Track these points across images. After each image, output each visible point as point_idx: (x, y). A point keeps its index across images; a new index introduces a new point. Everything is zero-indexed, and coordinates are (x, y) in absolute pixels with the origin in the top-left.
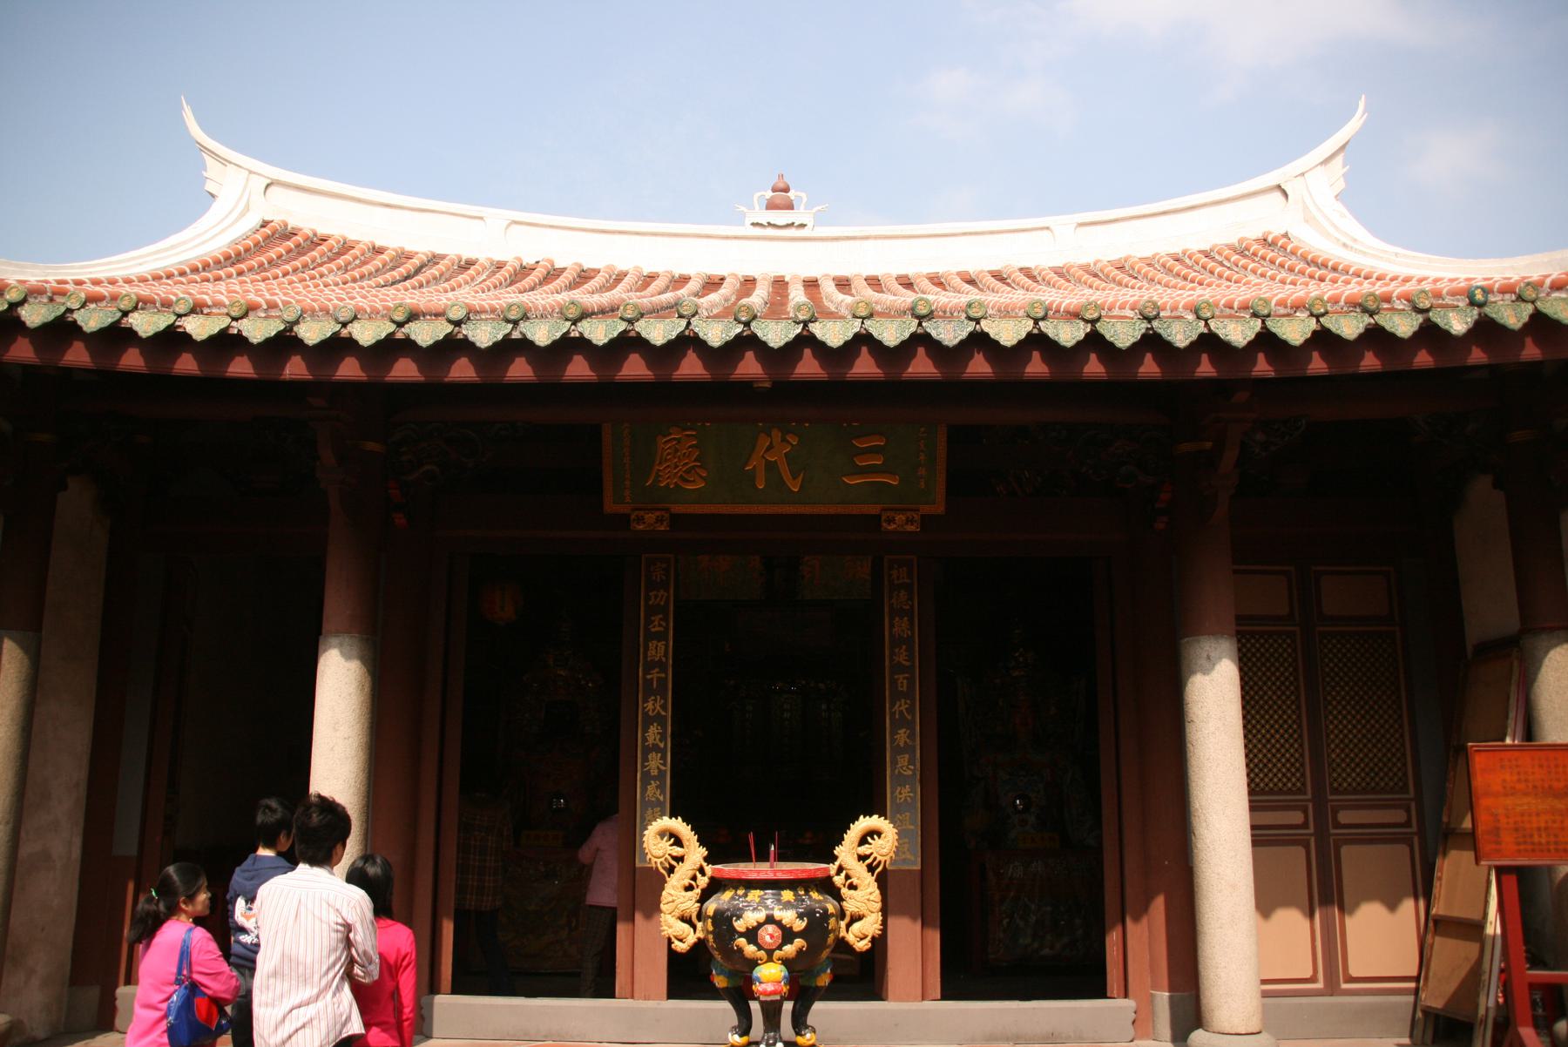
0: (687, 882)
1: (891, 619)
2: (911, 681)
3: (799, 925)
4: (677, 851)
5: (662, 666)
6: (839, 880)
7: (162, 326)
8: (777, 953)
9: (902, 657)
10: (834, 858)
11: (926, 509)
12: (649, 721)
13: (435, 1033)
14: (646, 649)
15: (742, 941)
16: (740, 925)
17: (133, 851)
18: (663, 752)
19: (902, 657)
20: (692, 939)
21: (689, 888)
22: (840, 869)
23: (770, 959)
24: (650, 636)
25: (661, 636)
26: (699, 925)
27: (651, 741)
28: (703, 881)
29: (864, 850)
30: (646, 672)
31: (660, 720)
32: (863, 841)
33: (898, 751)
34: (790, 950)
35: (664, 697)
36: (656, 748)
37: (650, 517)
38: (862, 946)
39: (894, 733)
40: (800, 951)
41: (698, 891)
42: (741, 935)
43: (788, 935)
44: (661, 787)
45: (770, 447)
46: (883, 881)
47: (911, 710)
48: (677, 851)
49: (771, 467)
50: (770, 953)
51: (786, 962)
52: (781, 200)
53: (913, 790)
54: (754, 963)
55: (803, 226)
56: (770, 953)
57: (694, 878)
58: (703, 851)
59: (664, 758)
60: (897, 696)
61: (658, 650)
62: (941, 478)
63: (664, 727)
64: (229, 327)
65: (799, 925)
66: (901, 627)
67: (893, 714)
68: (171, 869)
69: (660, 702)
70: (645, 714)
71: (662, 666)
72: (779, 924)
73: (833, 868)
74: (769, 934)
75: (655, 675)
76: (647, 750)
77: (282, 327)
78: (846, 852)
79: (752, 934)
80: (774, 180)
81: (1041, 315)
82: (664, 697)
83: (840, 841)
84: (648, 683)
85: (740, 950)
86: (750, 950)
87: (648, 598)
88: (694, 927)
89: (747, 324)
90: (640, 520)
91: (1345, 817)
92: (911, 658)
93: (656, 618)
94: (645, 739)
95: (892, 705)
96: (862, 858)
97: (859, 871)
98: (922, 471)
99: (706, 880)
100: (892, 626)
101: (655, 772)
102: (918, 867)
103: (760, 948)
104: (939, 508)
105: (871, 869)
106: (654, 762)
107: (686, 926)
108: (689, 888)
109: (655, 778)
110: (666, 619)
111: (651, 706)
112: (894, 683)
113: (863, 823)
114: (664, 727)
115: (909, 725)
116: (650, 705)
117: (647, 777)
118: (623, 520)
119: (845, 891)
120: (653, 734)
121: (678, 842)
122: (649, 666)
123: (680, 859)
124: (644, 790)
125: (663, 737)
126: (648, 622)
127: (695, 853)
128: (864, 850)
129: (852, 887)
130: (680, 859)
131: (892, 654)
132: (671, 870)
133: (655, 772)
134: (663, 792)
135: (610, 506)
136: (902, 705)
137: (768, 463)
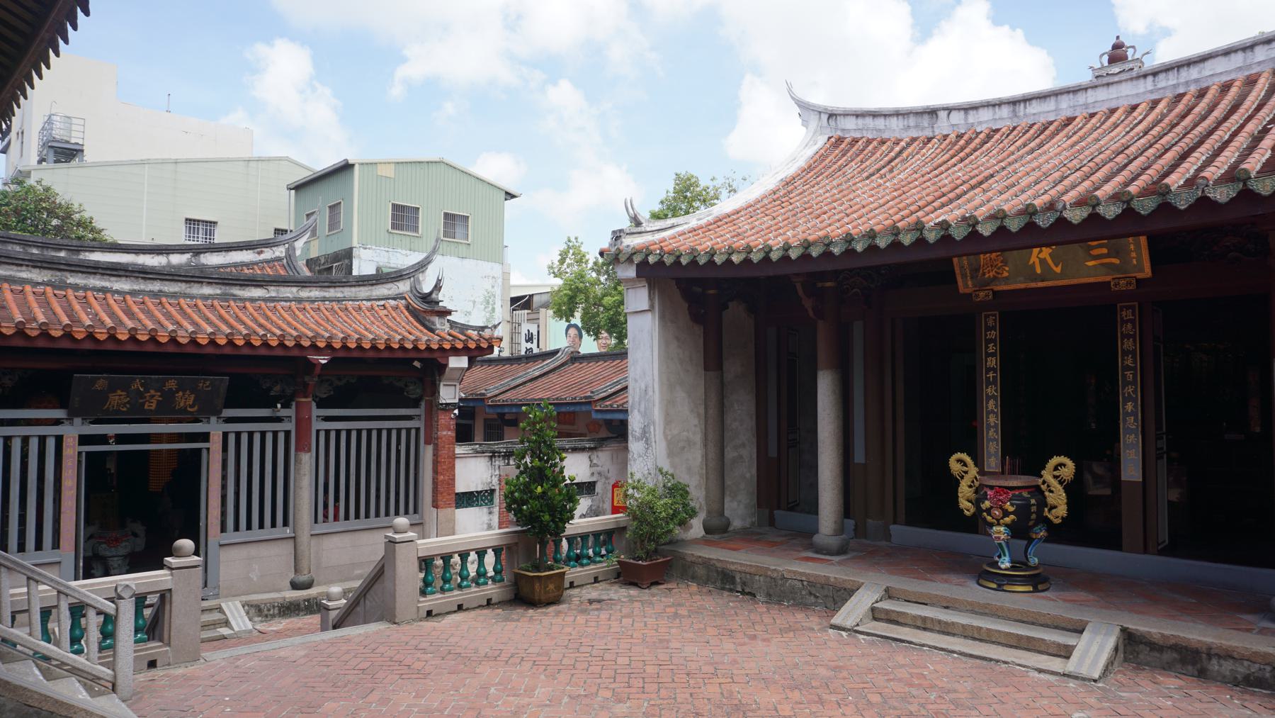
2: (1135, 376)
4: (965, 469)
5: (994, 370)
6: (1044, 487)
9: (1129, 362)
11: (1140, 276)
12: (989, 398)
13: (346, 246)
17: (775, 455)
19: (1129, 362)
22: (1044, 482)
23: (999, 524)
24: (988, 355)
25: (993, 355)
28: (977, 484)
29: (1056, 473)
32: (1056, 469)
33: (1127, 414)
36: (992, 412)
37: (982, 294)
38: (1058, 521)
39: (1125, 404)
43: (1006, 513)
47: (1135, 391)
48: (965, 469)
49: (1043, 262)
51: (1006, 525)
53: (1137, 436)
54: (991, 525)
58: (213, 419)
60: (1126, 384)
61: (992, 362)
66: (1128, 344)
68: (1258, 430)
71: (994, 370)
73: (1041, 481)
75: (991, 375)
76: (988, 413)
78: (1047, 474)
83: (1044, 468)
90: (977, 296)
96: (1056, 477)
97: (1054, 483)
98: (1134, 255)
104: (1147, 272)
105: (1061, 483)
111: (991, 390)
112: (1124, 376)
113: (1056, 460)
115: (1135, 400)
117: (989, 427)
119: (1047, 493)
121: (965, 465)
122: (988, 370)
123: (966, 472)
126: (987, 347)
127: (973, 471)
128: (1056, 473)
129: (1051, 491)
130: (966, 472)
132: (962, 477)
135: (962, 290)
136: (1130, 389)
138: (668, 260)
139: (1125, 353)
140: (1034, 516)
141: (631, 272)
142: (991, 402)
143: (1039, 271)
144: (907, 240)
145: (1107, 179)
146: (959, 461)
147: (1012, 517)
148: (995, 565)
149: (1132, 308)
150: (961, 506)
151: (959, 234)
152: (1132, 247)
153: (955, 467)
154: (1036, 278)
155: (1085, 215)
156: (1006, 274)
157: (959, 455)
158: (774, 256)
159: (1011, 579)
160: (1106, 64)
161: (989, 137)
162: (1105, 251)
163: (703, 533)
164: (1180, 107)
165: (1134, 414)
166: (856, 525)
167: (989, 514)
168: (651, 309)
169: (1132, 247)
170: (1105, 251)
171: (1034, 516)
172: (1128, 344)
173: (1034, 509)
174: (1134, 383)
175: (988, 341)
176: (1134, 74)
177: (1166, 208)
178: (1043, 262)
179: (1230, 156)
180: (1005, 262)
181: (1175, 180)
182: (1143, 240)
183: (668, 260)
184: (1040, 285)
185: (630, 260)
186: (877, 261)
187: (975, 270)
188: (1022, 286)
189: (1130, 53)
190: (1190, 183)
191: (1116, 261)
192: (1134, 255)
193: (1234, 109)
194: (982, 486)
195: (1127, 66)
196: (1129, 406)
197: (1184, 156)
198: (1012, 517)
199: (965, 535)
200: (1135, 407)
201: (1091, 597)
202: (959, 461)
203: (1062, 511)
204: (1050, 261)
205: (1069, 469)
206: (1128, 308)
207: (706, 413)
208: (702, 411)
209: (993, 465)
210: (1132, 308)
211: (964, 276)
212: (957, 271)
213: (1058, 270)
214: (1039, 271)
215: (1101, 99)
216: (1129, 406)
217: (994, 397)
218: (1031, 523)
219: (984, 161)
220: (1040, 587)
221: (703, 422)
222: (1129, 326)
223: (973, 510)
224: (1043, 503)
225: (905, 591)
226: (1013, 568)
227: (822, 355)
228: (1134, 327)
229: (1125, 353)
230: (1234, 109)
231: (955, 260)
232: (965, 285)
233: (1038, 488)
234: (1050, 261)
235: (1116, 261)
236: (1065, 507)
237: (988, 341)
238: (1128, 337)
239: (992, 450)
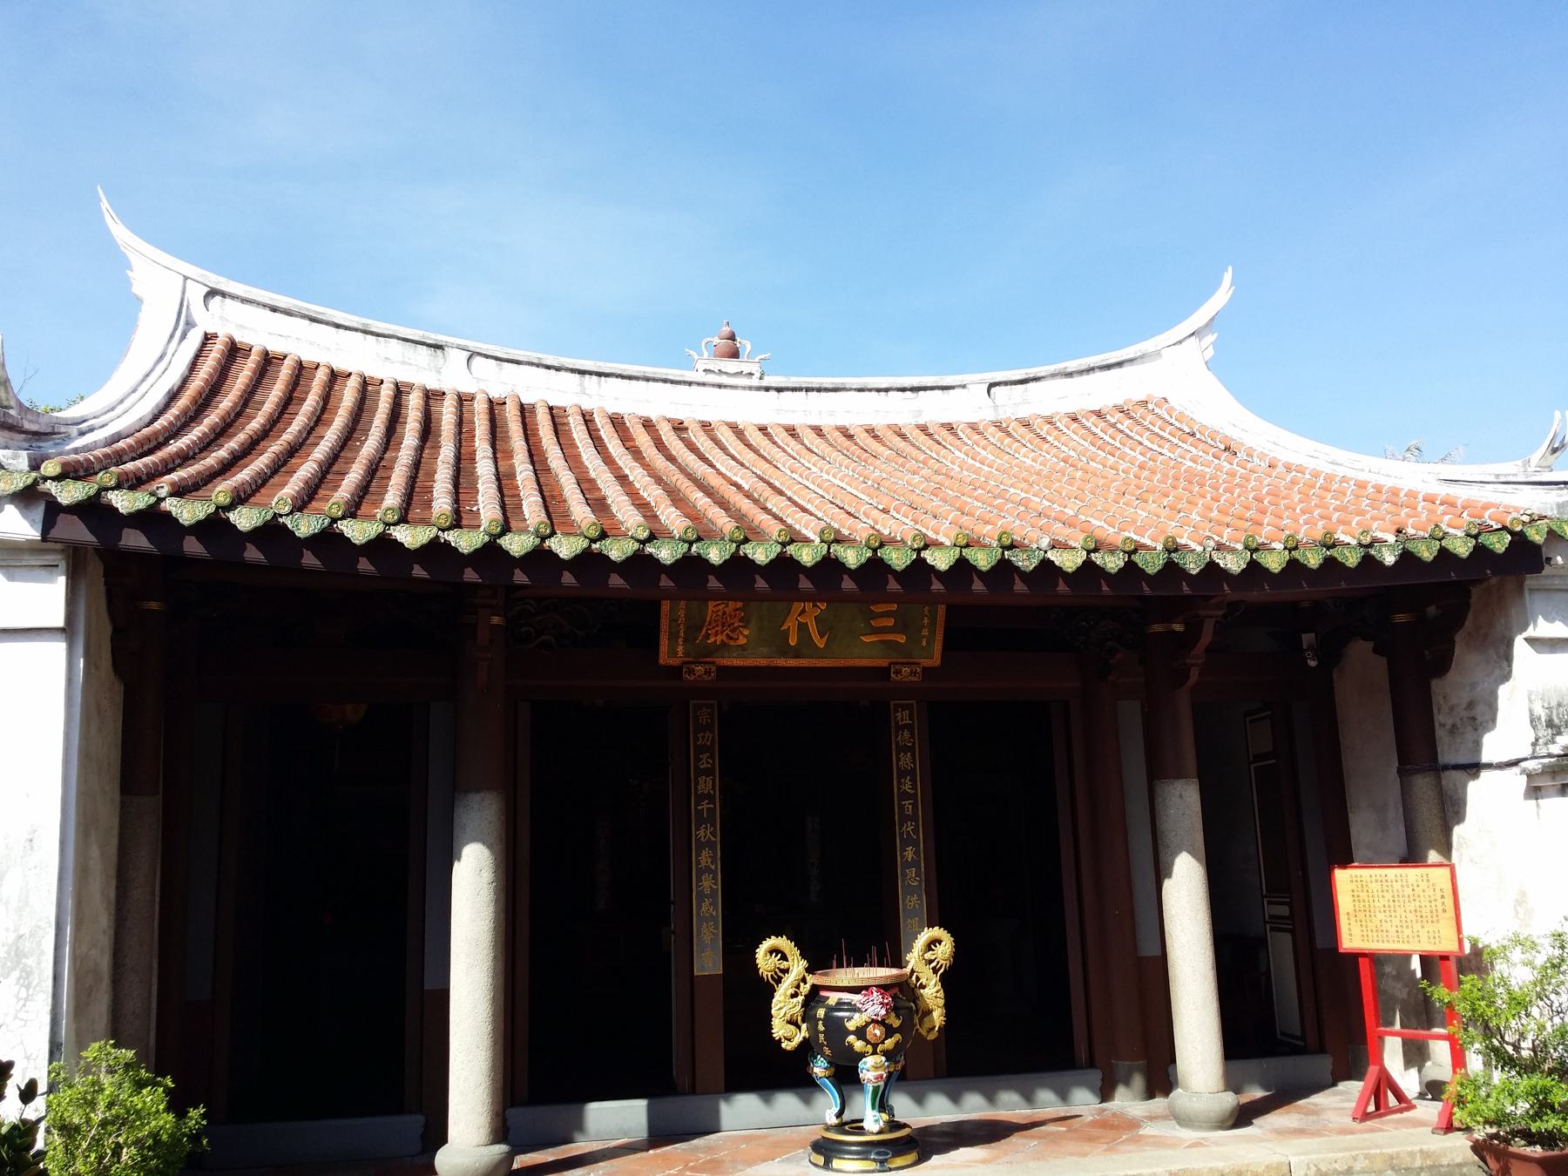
0: (792, 991)
1: (898, 754)
2: (915, 806)
5: (711, 798)
7: (373, 535)
9: (907, 787)
11: (927, 663)
12: (701, 846)
14: (697, 784)
15: (851, 1038)
16: (851, 1026)
18: (714, 872)
19: (907, 787)
20: (798, 1040)
21: (794, 995)
23: (875, 1053)
24: (699, 773)
25: (709, 772)
26: (804, 1026)
27: (703, 863)
28: (805, 989)
29: (928, 956)
31: (710, 845)
33: (907, 865)
34: (889, 1043)
35: (713, 825)
36: (708, 870)
37: (700, 669)
39: (904, 850)
40: (897, 1043)
41: (800, 998)
44: (714, 904)
45: (803, 611)
47: (916, 831)
48: (784, 965)
49: (803, 628)
50: (875, 1046)
51: (885, 1053)
53: (920, 898)
54: (862, 1055)
55: (751, 374)
56: (875, 1046)
57: (798, 987)
58: (804, 963)
59: (715, 878)
61: (706, 785)
62: (939, 637)
63: (715, 852)
64: (437, 537)
66: (906, 761)
67: (901, 835)
70: (698, 840)
71: (711, 798)
75: (705, 805)
76: (700, 872)
77: (487, 538)
78: (913, 958)
79: (861, 1033)
80: (726, 330)
81: (1092, 546)
82: (713, 825)
85: (851, 1046)
86: (859, 1045)
88: (799, 1028)
89: (875, 550)
92: (914, 787)
93: (704, 756)
94: (698, 863)
95: (901, 827)
98: (925, 632)
99: (808, 986)
100: (898, 760)
103: (868, 1042)
104: (936, 661)
105: (935, 971)
107: (792, 1027)
108: (794, 995)
110: (712, 757)
112: (901, 807)
115: (916, 844)
118: (676, 672)
120: (705, 855)
121: (784, 958)
123: (786, 971)
124: (699, 907)
126: (698, 760)
127: (797, 966)
128: (928, 956)
130: (786, 971)
131: (899, 783)
132: (779, 981)
134: (715, 909)
135: (664, 659)
137: (800, 624)
139: (903, 774)
142: (705, 853)
144: (1313, 560)
146: (774, 951)
147: (898, 1036)
149: (909, 707)
153: (764, 961)
154: (786, 651)
156: (742, 641)
157: (772, 942)
162: (890, 622)
165: (915, 863)
166: (426, 1126)
168: (67, 631)
170: (890, 622)
172: (906, 761)
174: (914, 818)
175: (700, 750)
176: (755, 382)
178: (803, 628)
180: (746, 622)
184: (792, 663)
186: (1264, 594)
187: (694, 627)
188: (763, 662)
192: (925, 632)
194: (816, 989)
196: (909, 853)
199: (333, 1122)
200: (917, 853)
202: (774, 951)
203: (938, 1017)
206: (904, 707)
210: (909, 707)
211: (673, 636)
216: (909, 853)
217: (710, 845)
222: (906, 734)
228: (912, 736)
229: (903, 774)
231: (666, 606)
232: (670, 652)
235: (902, 639)
237: (700, 750)
238: (905, 749)
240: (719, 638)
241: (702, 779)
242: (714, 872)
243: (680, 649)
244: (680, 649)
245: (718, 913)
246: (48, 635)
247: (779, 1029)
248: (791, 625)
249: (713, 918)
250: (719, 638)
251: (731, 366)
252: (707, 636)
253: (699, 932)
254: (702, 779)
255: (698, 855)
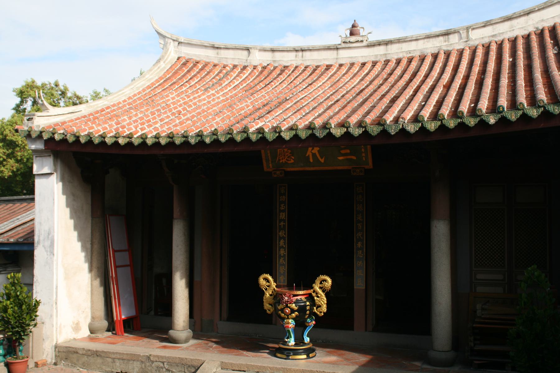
3: (296, 308)
5: (284, 221)
6: (314, 294)
8: (290, 316)
10: (312, 288)
12: (280, 238)
14: (279, 215)
15: (280, 312)
22: (314, 292)
23: (288, 318)
25: (283, 211)
30: (279, 223)
36: (282, 247)
37: (278, 172)
40: (297, 316)
42: (280, 310)
43: (293, 311)
44: (284, 260)
46: (327, 295)
49: (314, 155)
51: (293, 319)
52: (43, 323)
56: (288, 316)
59: (285, 250)
61: (283, 216)
63: (285, 240)
65: (296, 308)
69: (284, 232)
70: (279, 236)
72: (289, 307)
74: (288, 311)
75: (282, 224)
76: (280, 248)
78: (317, 287)
83: (314, 282)
84: (280, 226)
85: (280, 315)
87: (280, 199)
91: (479, 276)
93: (282, 205)
94: (279, 244)
96: (320, 288)
97: (320, 291)
98: (364, 155)
101: (282, 255)
102: (364, 288)
104: (370, 165)
105: (323, 291)
106: (282, 252)
109: (282, 257)
111: (281, 234)
114: (285, 240)
116: (281, 233)
119: (316, 298)
120: (282, 241)
122: (281, 221)
124: (279, 261)
125: (285, 243)
126: (280, 206)
127: (274, 285)
129: (318, 297)
133: (282, 255)
134: (285, 261)
135: (265, 169)
136: (360, 234)
138: (71, 139)
140: (308, 312)
141: (39, 146)
142: (282, 241)
143: (311, 160)
145: (354, 111)
148: (285, 343)
150: (265, 308)
151: (271, 137)
152: (363, 150)
153: (262, 281)
155: (343, 132)
156: (292, 161)
158: (149, 142)
159: (296, 352)
160: (348, 35)
161: (282, 71)
162: (348, 151)
163: (89, 333)
164: (388, 70)
167: (283, 312)
169: (363, 150)
170: (348, 151)
171: (308, 312)
173: (308, 308)
177: (384, 133)
178: (314, 155)
179: (414, 106)
181: (389, 118)
182: (369, 147)
183: (71, 139)
185: (40, 136)
188: (301, 169)
189: (361, 31)
190: (396, 120)
191: (354, 158)
192: (364, 155)
193: (414, 75)
195: (360, 39)
196: (359, 245)
197: (393, 101)
198: (297, 313)
200: (363, 245)
201: (333, 358)
203: (324, 309)
204: (318, 155)
205: (329, 282)
207: (92, 247)
208: (89, 246)
209: (282, 281)
212: (263, 157)
213: (322, 161)
214: (311, 160)
215: (345, 56)
216: (359, 245)
218: (307, 316)
219: (278, 88)
220: (311, 355)
221: (89, 254)
223: (272, 310)
224: (313, 303)
225: (231, 364)
226: (296, 345)
227: (177, 211)
230: (414, 75)
232: (268, 166)
233: (310, 294)
234: (318, 155)
235: (354, 158)
236: (325, 306)
239: (282, 272)
240: (284, 161)
241: (281, 214)
242: (285, 248)
243: (271, 165)
244: (271, 165)
245: (286, 263)
246: (42, 177)
247: (267, 306)
248: (309, 153)
249: (283, 265)
250: (284, 161)
251: (353, 39)
252: (279, 160)
253: (279, 269)
254: (281, 214)
255: (279, 241)
